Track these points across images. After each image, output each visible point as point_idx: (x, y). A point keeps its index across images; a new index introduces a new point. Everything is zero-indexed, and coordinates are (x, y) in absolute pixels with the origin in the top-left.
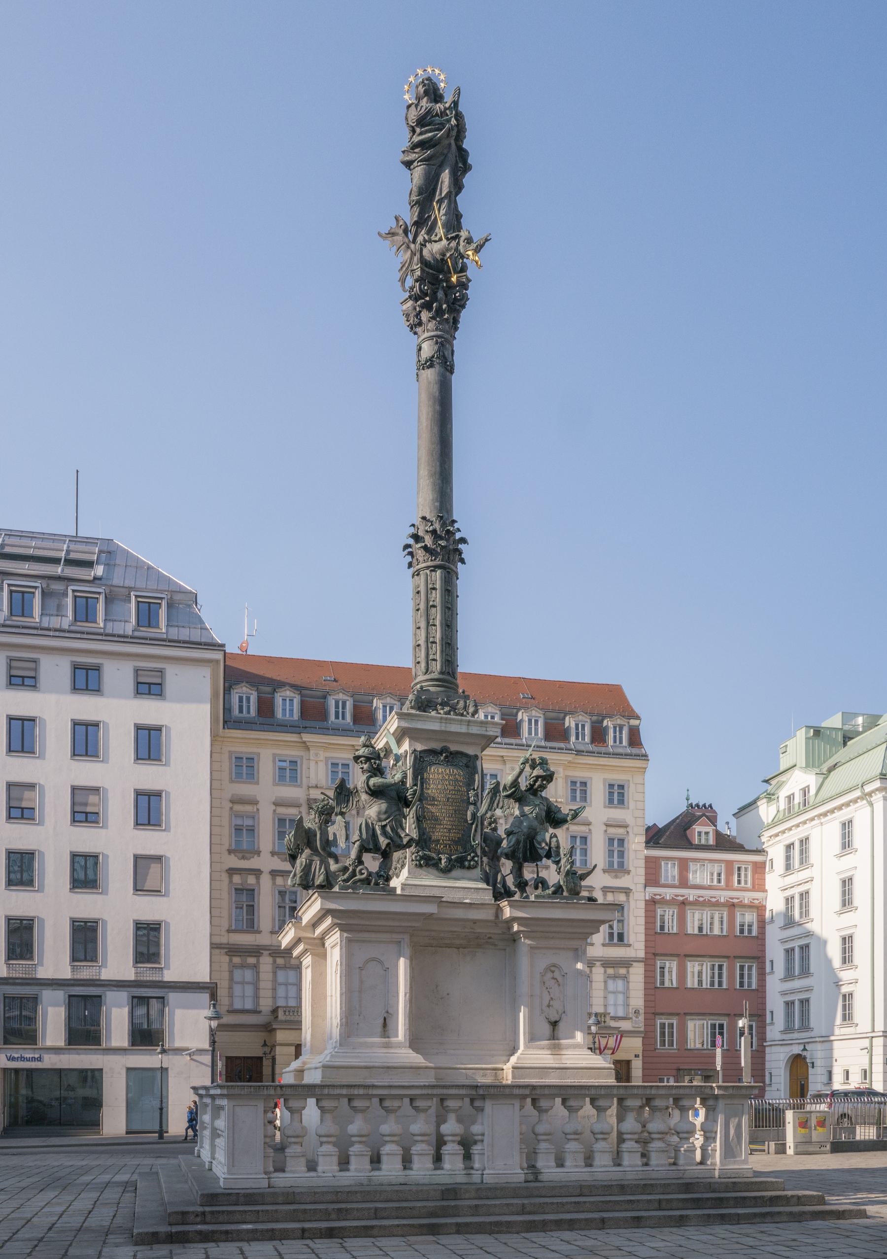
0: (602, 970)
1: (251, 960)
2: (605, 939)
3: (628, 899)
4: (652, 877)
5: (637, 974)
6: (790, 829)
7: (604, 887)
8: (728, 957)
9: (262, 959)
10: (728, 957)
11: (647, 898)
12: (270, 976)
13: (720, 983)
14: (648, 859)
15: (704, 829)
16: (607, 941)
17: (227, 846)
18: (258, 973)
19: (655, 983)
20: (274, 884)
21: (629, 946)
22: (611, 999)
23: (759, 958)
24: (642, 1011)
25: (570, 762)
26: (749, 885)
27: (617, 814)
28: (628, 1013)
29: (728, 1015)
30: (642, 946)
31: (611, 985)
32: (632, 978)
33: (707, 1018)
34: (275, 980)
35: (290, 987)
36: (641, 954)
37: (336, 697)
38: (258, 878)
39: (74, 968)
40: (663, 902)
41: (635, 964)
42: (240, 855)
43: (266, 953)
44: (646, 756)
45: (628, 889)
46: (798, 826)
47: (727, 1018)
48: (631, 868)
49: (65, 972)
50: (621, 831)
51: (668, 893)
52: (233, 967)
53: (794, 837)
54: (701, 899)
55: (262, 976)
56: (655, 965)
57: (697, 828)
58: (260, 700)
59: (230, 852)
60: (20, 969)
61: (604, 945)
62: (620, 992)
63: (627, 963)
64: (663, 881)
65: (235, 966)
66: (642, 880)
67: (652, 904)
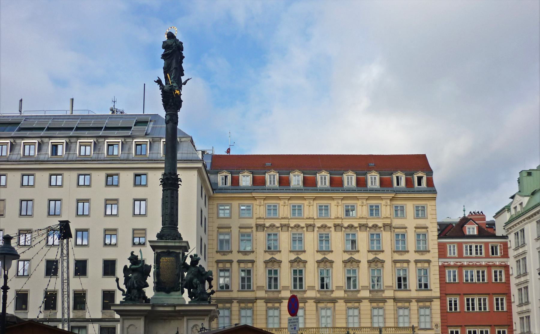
0: (416, 304)
1: (228, 305)
2: (239, 288)
3: (429, 267)
4: (442, 253)
5: (436, 305)
6: (515, 225)
7: (416, 260)
8: (489, 294)
9: (233, 305)
10: (489, 294)
11: (440, 264)
12: (237, 313)
13: (485, 309)
14: (440, 244)
15: (471, 226)
16: (418, 288)
17: (215, 250)
18: (231, 311)
19: (446, 309)
20: (239, 267)
21: (431, 290)
22: (422, 319)
23: (508, 294)
24: (440, 325)
25: (393, 197)
26: (456, 255)
27: (421, 222)
28: (432, 326)
29: (491, 326)
30: (438, 290)
31: (422, 311)
32: (433, 307)
33: (478, 327)
34: (240, 314)
35: (380, 317)
36: (438, 294)
37: (397, 175)
38: (231, 265)
39: (103, 313)
40: (449, 266)
41: (339, 301)
42: (222, 253)
43: (235, 301)
44: (435, 191)
45: (429, 260)
46: (518, 223)
47: (490, 328)
48: (430, 249)
49: (99, 315)
50: (424, 230)
51: (452, 262)
52: (268, 308)
53: (518, 229)
54: (471, 264)
55: (233, 313)
56: (446, 300)
57: (467, 226)
58: (232, 178)
59: (217, 252)
60: (79, 314)
61: (416, 290)
62: (226, 317)
63: (430, 300)
64: (448, 255)
65: (349, 308)
66: (437, 255)
67: (442, 268)
